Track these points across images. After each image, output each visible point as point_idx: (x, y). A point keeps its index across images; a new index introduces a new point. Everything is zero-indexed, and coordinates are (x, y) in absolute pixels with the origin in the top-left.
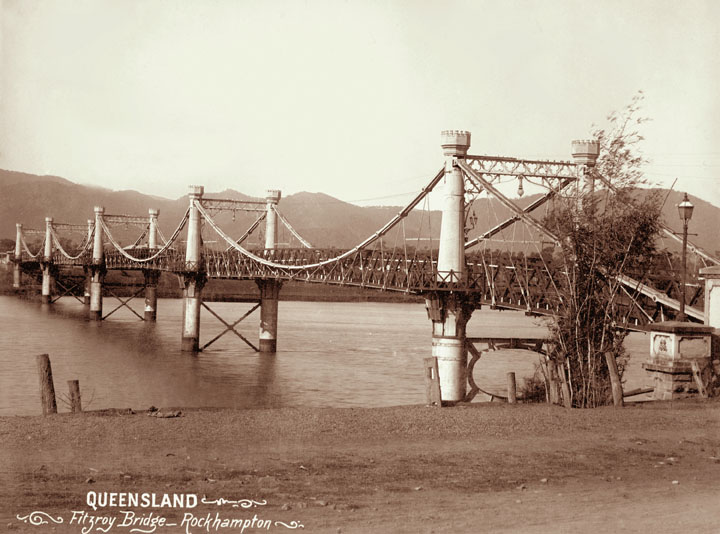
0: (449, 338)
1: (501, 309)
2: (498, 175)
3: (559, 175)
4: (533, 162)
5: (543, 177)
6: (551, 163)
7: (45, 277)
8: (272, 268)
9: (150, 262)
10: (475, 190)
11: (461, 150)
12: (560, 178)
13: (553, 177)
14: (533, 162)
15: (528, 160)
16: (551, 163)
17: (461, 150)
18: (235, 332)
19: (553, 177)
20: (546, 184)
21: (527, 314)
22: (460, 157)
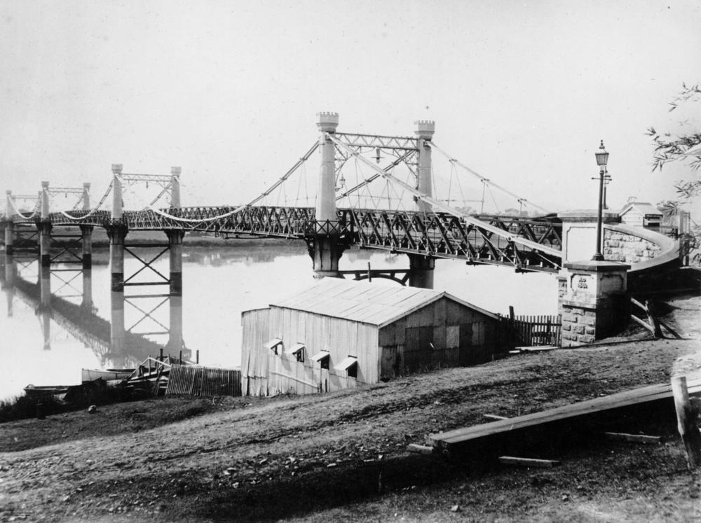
0: (327, 271)
1: (367, 249)
2: (360, 147)
3: (405, 147)
4: (351, 135)
5: (394, 149)
6: (399, 138)
7: (6, 233)
8: (189, 223)
9: (85, 220)
10: (343, 158)
11: (330, 128)
12: (406, 149)
13: (401, 149)
14: (351, 135)
15: (382, 135)
16: (399, 138)
17: (330, 128)
18: (151, 268)
19: (401, 149)
20: (395, 154)
21: (468, 263)
22: (330, 133)
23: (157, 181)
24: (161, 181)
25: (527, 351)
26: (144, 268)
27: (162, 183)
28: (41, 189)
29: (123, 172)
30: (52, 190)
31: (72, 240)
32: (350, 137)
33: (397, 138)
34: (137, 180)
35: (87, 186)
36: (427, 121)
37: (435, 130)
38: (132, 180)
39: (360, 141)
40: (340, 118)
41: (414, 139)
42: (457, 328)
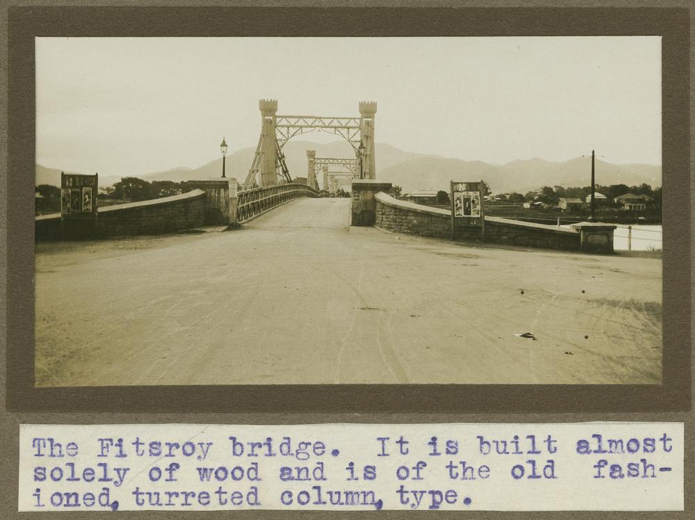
27: (344, 131)
29: (277, 114)
38: (294, 126)
39: (327, 161)
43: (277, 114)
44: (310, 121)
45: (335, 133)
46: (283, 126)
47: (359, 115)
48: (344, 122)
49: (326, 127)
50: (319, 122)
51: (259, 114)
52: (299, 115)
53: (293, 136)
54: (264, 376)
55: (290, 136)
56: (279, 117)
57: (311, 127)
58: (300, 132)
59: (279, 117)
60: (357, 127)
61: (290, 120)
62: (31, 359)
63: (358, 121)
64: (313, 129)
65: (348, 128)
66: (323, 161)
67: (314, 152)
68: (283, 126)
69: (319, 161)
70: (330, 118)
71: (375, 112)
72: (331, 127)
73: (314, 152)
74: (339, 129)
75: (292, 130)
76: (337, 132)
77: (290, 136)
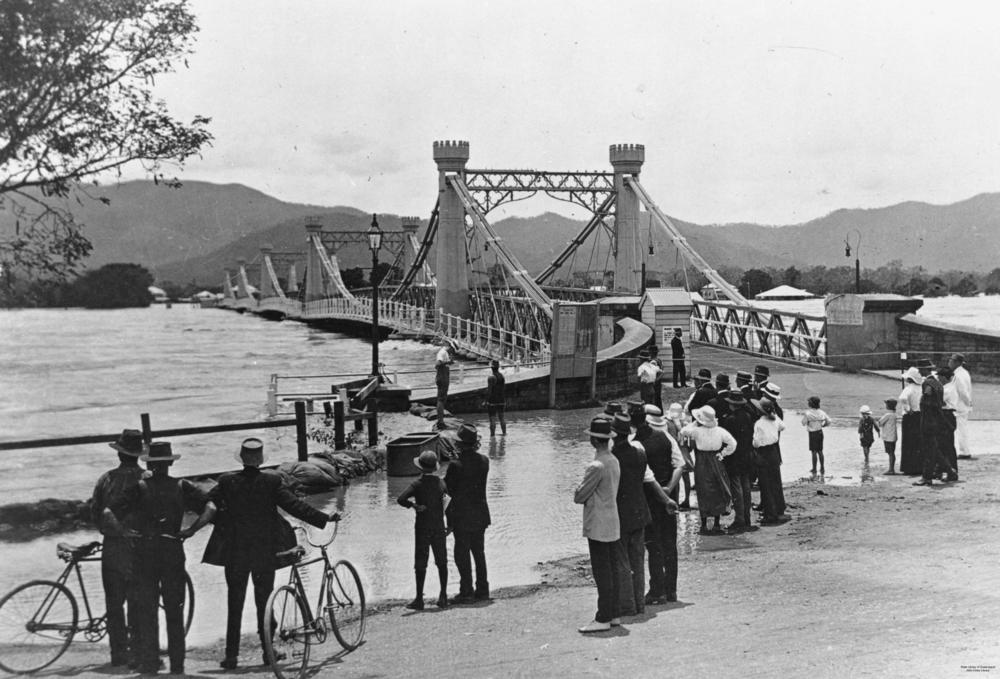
23: (572, 191)
24: (585, 190)
25: (878, 375)
26: (336, 526)
27: (587, 197)
28: (173, 187)
29: (469, 166)
30: (480, 181)
31: (272, 589)
32: (523, 176)
33: (578, 174)
34: (510, 190)
35: (627, 160)
36: (626, 145)
37: (371, 212)
38: (497, 189)
39: (511, 182)
40: (470, 147)
41: (609, 175)
42: (353, 422)
43: (469, 166)
44: (526, 180)
45: (571, 201)
46: (478, 189)
47: (611, 169)
48: (586, 181)
49: (554, 189)
50: (538, 180)
51: (433, 168)
52: (507, 169)
53: (496, 205)
54: (43, 433)
55: (491, 206)
56: (471, 172)
57: (528, 189)
58: (508, 198)
59: (471, 172)
60: (608, 190)
61: (492, 178)
62: (298, 437)
63: (610, 179)
64: (531, 193)
65: (594, 192)
66: (495, 180)
67: (464, 146)
68: (478, 189)
69: (480, 181)
70: (561, 174)
71: (641, 163)
72: (564, 190)
73: (464, 146)
74: (578, 194)
75: (495, 196)
76: (575, 199)
77: (491, 206)
